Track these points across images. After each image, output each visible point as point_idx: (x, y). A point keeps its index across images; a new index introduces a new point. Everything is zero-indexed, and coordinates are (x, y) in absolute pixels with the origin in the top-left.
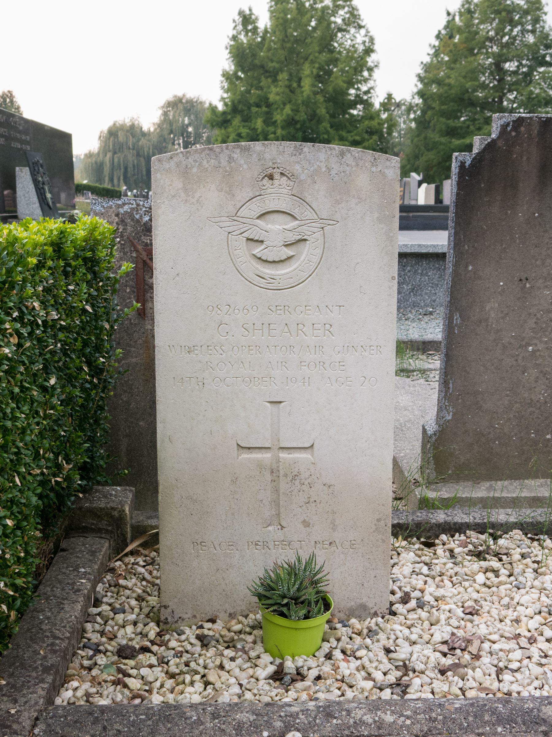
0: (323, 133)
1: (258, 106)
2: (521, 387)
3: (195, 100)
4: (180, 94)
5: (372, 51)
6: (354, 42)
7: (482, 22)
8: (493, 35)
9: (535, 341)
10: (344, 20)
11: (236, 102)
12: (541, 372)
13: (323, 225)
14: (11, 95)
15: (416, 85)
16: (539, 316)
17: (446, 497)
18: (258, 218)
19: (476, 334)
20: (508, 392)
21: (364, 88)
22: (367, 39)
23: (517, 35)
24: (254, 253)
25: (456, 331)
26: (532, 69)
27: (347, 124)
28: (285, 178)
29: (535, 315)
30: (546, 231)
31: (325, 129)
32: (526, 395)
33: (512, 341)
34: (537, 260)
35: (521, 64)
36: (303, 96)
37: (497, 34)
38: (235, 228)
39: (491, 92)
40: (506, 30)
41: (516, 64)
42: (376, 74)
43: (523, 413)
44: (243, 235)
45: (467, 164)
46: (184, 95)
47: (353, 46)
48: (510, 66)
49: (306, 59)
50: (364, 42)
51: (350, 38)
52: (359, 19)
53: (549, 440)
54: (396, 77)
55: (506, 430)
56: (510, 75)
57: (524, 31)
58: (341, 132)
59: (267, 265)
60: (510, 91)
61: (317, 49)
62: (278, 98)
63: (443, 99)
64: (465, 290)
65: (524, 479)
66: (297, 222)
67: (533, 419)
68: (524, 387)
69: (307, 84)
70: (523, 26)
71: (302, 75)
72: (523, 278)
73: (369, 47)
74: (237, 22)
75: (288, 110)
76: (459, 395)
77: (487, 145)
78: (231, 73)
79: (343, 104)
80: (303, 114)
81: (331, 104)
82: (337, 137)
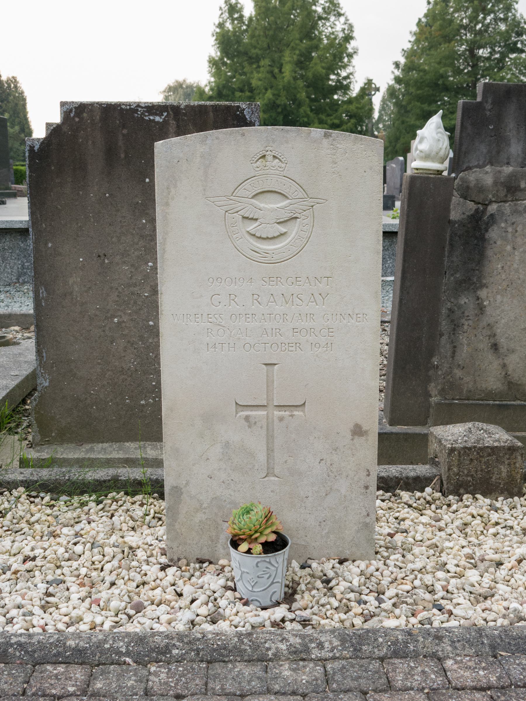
0: (303, 117)
1: (242, 91)
2: (111, 356)
3: (195, 85)
4: (181, 79)
5: (352, 38)
6: (334, 30)
7: (456, 10)
8: (468, 23)
9: (119, 313)
10: (324, 9)
11: (221, 86)
12: (129, 342)
13: (313, 204)
14: (15, 80)
15: (393, 72)
16: (120, 289)
17: (44, 458)
19: (63, 307)
20: (99, 361)
21: (344, 74)
22: (346, 27)
23: (489, 24)
24: (248, 230)
25: (43, 304)
26: (504, 56)
28: (277, 160)
29: (117, 289)
30: (118, 211)
31: (305, 112)
32: (117, 364)
33: (98, 313)
34: (112, 238)
35: (494, 50)
36: (283, 81)
37: (471, 22)
39: (466, 77)
40: (480, 18)
41: (489, 50)
43: (116, 380)
45: (36, 148)
46: (184, 81)
47: (333, 33)
48: (483, 52)
49: (288, 46)
50: (343, 30)
51: (330, 26)
52: (339, 7)
53: (143, 405)
54: (375, 63)
55: (102, 396)
56: (483, 61)
57: (496, 20)
58: (320, 116)
60: (483, 76)
61: (297, 36)
62: (260, 83)
63: (419, 84)
64: (47, 265)
65: (124, 442)
67: (126, 386)
68: (114, 356)
69: (287, 69)
70: (495, 14)
71: (283, 62)
72: (101, 254)
73: (348, 34)
74: (224, 10)
76: (53, 363)
77: (52, 130)
78: (217, 58)
79: (323, 89)
80: (284, 98)
81: (311, 89)
82: (316, 121)
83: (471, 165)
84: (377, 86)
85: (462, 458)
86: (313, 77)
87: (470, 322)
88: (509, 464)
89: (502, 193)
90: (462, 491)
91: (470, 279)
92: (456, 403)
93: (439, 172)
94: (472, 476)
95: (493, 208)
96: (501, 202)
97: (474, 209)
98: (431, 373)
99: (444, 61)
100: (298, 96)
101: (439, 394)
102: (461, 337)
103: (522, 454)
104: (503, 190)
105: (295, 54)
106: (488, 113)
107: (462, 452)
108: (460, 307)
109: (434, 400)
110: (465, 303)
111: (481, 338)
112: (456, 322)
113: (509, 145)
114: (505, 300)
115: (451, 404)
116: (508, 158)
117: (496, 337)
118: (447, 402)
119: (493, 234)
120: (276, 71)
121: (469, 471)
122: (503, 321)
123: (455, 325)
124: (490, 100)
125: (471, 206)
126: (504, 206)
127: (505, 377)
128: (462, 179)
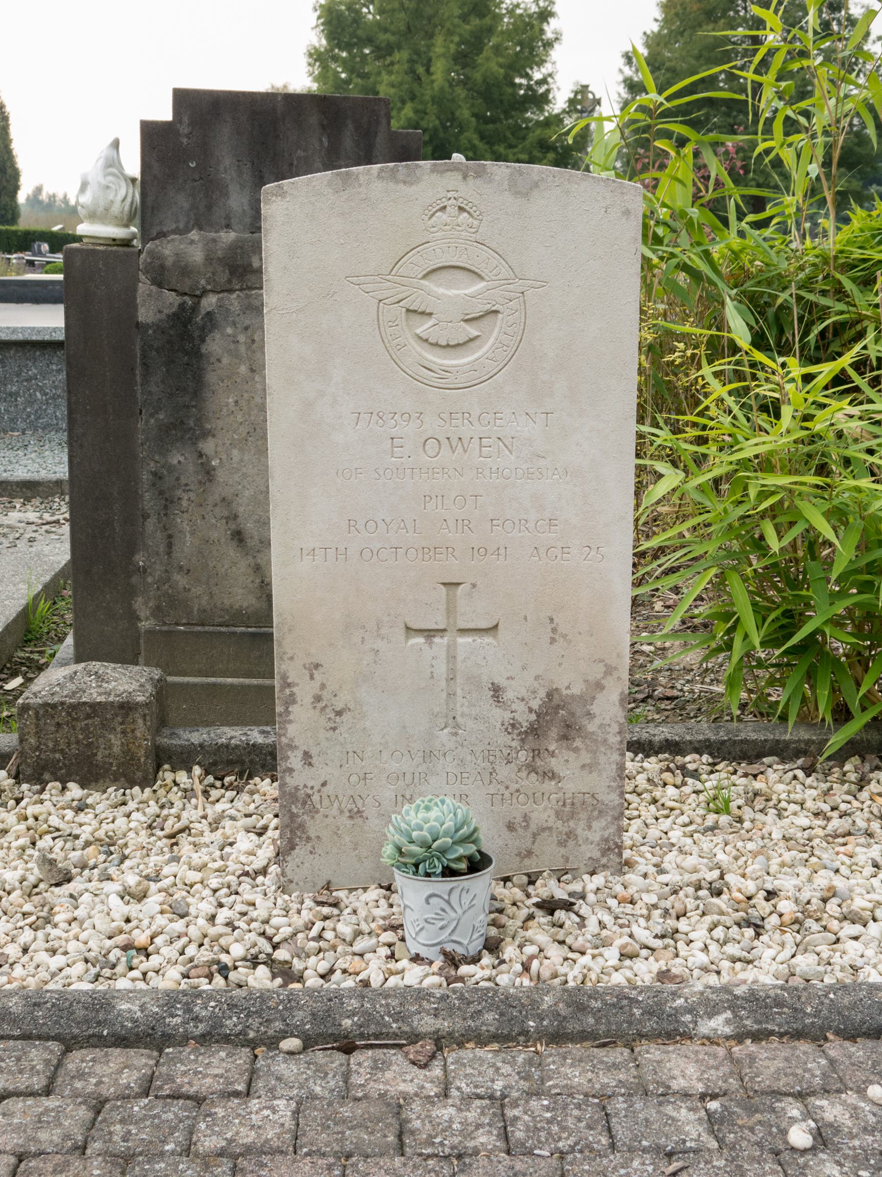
5: (551, 14)
15: (621, 71)
18: (425, 277)
21: (537, 75)
27: (508, 134)
28: (465, 214)
31: (470, 141)
36: (433, 89)
38: (387, 293)
42: (556, 53)
44: (401, 304)
58: (496, 147)
59: (437, 350)
61: (457, 12)
62: (392, 91)
66: (483, 284)
69: (439, 67)
73: (546, 8)
75: (408, 111)
80: (434, 118)
83: (165, 230)
84: (597, 97)
85: (42, 722)
86: (484, 81)
87: (192, 495)
88: (124, 732)
89: (223, 277)
90: (47, 776)
91: (182, 423)
92: (180, 631)
93: (126, 243)
94: (62, 751)
95: (210, 302)
96: (222, 291)
97: (176, 304)
98: (135, 580)
99: (705, 53)
100: (457, 114)
101: (152, 614)
102: (179, 520)
103: (145, 715)
104: (224, 271)
105: (452, 41)
106: (185, 141)
107: (41, 712)
108: (171, 469)
109: (145, 625)
110: (179, 462)
111: (214, 521)
112: (167, 495)
113: (226, 195)
114: (246, 457)
115: (169, 633)
116: (228, 217)
117: (239, 520)
118: (165, 628)
119: (214, 345)
120: (421, 70)
121: (56, 743)
122: (247, 493)
123: (166, 500)
124: (186, 119)
125: (171, 299)
126: (229, 299)
127: (262, 587)
128: (151, 253)
